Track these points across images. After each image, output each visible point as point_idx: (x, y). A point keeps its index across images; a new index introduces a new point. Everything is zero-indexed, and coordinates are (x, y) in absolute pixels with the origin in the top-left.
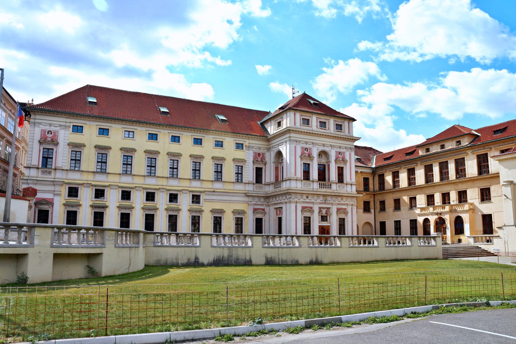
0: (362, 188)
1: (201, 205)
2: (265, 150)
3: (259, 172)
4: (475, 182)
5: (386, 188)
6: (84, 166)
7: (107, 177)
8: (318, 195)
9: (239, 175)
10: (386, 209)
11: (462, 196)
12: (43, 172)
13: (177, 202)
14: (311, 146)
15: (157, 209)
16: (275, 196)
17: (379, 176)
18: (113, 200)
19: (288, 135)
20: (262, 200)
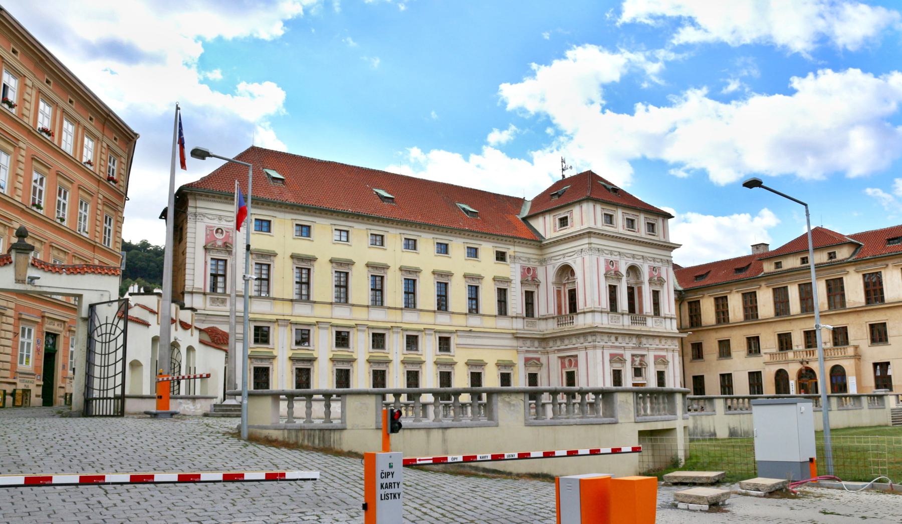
0: (686, 321)
1: (452, 354)
2: (537, 263)
3: (529, 297)
4: (862, 315)
5: (703, 324)
6: (388, 301)
7: (312, 308)
8: (630, 335)
9: (304, 286)
10: (705, 356)
11: (840, 336)
12: (213, 301)
13: (417, 350)
14: (617, 258)
15: (354, 360)
16: (562, 338)
17: (690, 303)
18: (323, 345)
19: (586, 241)
20: (536, 344)
